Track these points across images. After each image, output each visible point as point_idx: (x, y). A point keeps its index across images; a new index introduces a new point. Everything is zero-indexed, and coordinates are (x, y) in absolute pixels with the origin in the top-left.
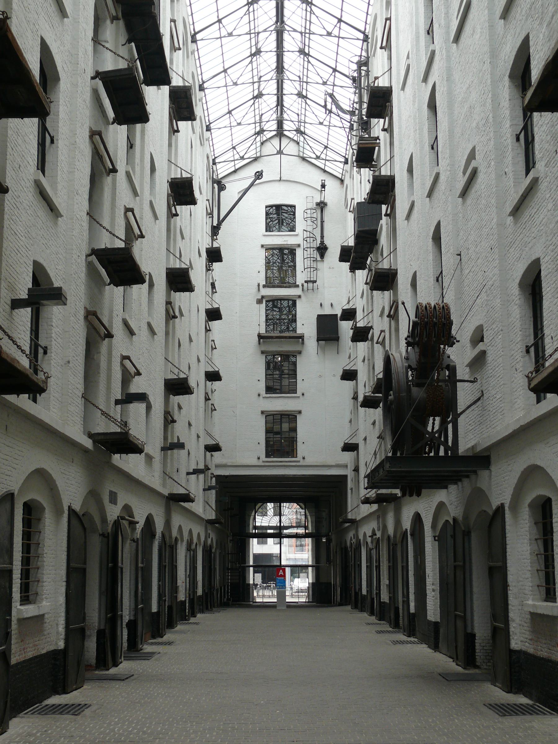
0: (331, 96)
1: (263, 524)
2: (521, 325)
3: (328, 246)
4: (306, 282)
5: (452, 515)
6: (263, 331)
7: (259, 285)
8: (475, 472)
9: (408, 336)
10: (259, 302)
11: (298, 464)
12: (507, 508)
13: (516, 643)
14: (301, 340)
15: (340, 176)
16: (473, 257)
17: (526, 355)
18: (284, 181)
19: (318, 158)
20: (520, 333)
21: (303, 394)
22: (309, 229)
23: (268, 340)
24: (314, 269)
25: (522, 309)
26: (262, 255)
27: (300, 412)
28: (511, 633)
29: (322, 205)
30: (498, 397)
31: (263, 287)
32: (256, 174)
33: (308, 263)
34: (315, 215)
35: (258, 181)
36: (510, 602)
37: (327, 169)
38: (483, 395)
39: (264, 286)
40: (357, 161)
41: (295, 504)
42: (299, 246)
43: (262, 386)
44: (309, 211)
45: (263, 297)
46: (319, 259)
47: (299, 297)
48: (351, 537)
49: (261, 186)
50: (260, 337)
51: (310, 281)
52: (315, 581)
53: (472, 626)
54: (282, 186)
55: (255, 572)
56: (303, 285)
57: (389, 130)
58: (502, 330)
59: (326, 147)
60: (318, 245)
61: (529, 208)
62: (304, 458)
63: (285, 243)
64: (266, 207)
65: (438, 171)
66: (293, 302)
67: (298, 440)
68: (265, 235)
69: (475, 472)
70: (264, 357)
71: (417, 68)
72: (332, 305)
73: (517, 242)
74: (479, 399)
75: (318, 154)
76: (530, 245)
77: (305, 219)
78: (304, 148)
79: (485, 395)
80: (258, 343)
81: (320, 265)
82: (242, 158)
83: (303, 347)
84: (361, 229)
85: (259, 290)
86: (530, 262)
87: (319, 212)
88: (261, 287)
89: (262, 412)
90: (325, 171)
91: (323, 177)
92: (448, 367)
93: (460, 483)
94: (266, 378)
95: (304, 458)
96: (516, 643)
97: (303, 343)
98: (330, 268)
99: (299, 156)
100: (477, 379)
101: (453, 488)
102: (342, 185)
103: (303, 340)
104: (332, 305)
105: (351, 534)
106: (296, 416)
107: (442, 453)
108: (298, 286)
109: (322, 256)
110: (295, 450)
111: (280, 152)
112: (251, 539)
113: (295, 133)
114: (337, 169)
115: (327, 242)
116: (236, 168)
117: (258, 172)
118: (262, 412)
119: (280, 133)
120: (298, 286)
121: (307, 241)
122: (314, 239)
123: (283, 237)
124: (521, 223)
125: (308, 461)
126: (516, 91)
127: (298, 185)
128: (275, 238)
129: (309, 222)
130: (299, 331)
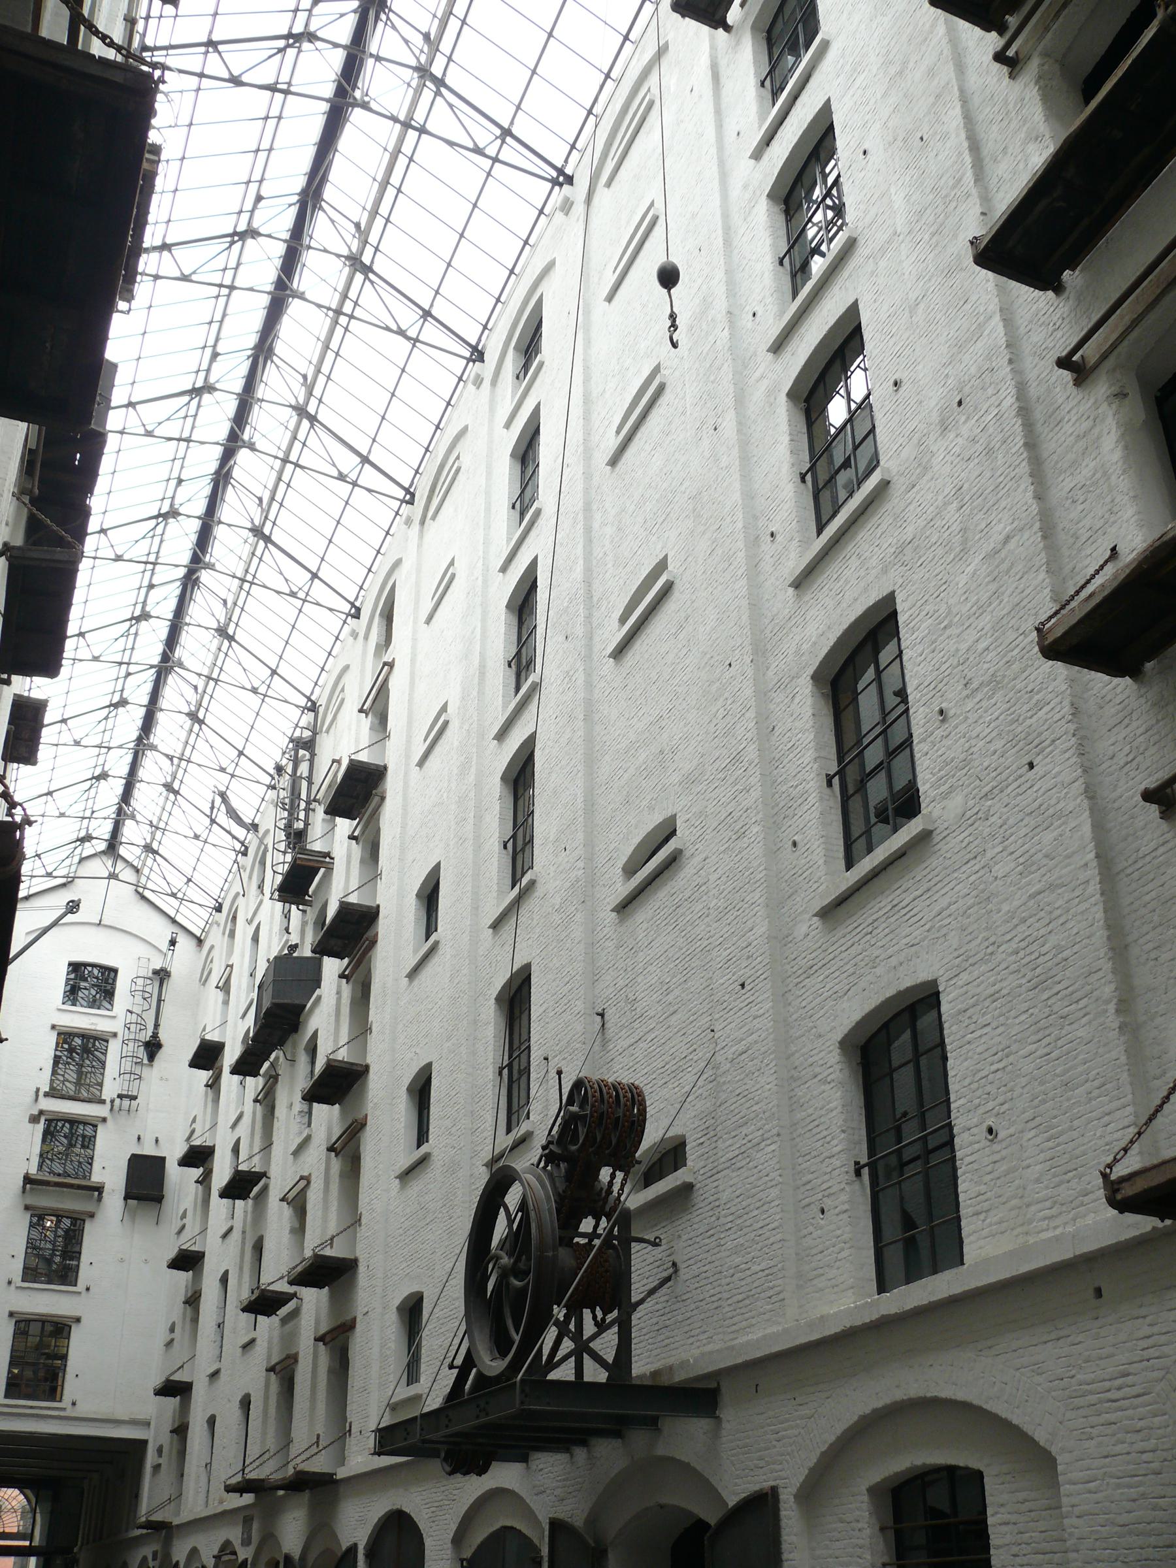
2: (845, 1121)
3: (162, 1042)
4: (120, 1096)
6: (33, 1170)
7: (38, 1090)
10: (34, 1119)
11: (62, 1414)
12: (787, 1499)
14: (96, 1193)
17: (855, 1179)
18: (106, 926)
20: (843, 1135)
21: (88, 1289)
22: (137, 1010)
23: (40, 1187)
24: (137, 1077)
25: (847, 1091)
26: (51, 1040)
27: (78, 1320)
29: (162, 975)
31: (45, 1096)
32: (68, 903)
33: (127, 1065)
34: (149, 989)
35: (70, 918)
37: (179, 918)
38: (676, 1271)
39: (46, 1095)
41: (17, 1492)
42: (115, 1035)
43: (18, 1266)
45: (41, 1112)
46: (146, 1061)
47: (104, 1120)
49: (66, 928)
51: (127, 1096)
54: (102, 933)
56: (112, 1101)
58: (778, 1135)
59: (315, 576)
60: (148, 1039)
61: (887, 892)
62: (74, 1404)
63: (93, 1027)
65: (534, 878)
66: (93, 1124)
67: (68, 1369)
68: (59, 1010)
70: (28, 1215)
71: (478, 720)
72: (157, 1141)
74: (668, 1279)
75: (295, 589)
77: (132, 993)
78: (148, 878)
79: (682, 1272)
80: (21, 1190)
81: (146, 1072)
82: (49, 875)
83: (99, 1205)
84: (276, 1001)
85: (36, 1100)
87: (157, 984)
88: (41, 1094)
90: (174, 921)
91: (175, 929)
93: (580, 1453)
94: (26, 1253)
95: (74, 1404)
98: (161, 1079)
100: (661, 1240)
102: (198, 948)
104: (157, 1141)
106: (70, 1327)
108: (103, 1102)
109: (151, 1057)
110: (59, 1389)
114: (194, 918)
115: (163, 1036)
116: (31, 893)
117: (72, 901)
118: (11, 1314)
120: (103, 1102)
121: (129, 1029)
122: (143, 1027)
123: (91, 1017)
124: (855, 925)
125: (83, 1410)
126: (823, 703)
128: (76, 1016)
129: (138, 999)
130: (96, 1177)
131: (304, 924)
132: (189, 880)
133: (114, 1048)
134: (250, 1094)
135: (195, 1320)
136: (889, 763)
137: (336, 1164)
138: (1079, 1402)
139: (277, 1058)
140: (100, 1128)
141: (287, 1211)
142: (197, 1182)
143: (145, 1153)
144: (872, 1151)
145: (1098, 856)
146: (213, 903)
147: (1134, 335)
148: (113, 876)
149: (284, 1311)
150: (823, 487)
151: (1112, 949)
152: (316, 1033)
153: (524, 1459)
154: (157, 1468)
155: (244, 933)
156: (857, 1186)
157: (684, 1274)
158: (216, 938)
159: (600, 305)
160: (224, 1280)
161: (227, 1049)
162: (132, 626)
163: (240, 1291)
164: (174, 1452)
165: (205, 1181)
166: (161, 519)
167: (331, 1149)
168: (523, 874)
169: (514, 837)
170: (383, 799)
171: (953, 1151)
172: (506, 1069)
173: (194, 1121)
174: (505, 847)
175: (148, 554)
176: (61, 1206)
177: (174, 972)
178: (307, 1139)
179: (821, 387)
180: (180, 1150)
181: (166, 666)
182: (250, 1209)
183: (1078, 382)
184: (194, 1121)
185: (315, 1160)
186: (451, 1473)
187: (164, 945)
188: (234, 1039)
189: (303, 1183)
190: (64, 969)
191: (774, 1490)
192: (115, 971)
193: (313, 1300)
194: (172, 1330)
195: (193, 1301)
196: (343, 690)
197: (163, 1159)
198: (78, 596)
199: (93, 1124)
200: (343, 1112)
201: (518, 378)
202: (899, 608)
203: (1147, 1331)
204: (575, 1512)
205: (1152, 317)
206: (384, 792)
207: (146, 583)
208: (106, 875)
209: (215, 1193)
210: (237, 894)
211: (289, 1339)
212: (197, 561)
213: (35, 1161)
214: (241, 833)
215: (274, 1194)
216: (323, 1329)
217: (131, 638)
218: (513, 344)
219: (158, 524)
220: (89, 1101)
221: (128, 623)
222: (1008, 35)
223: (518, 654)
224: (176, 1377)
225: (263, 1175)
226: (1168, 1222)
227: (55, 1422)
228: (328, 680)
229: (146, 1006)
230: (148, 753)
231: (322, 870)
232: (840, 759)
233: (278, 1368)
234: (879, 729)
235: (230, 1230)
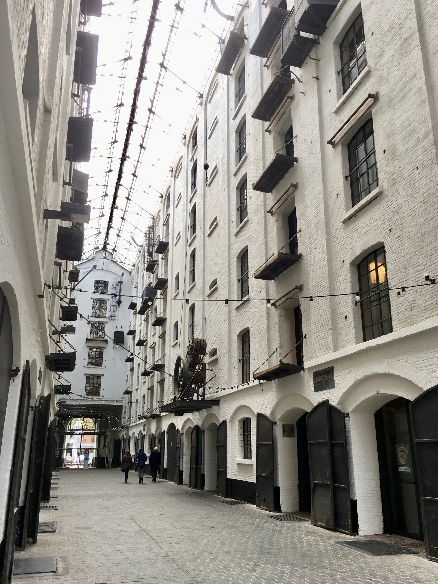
0: (132, 238)
1: (74, 428)
3: (122, 301)
4: (111, 316)
5: (195, 424)
6: (89, 337)
7: (89, 316)
8: (211, 407)
9: (188, 351)
12: (227, 422)
13: (230, 476)
15: (130, 271)
16: (213, 321)
19: (122, 262)
21: (105, 367)
27: (103, 375)
28: (227, 473)
29: (121, 283)
30: (225, 378)
33: (112, 308)
34: (117, 287)
36: (227, 460)
37: (124, 267)
38: (215, 376)
39: (91, 316)
40: (146, 269)
42: (109, 300)
44: (115, 285)
46: (117, 306)
47: (107, 322)
48: (123, 435)
50: (87, 339)
51: (113, 316)
52: (96, 456)
53: (204, 470)
55: (67, 452)
56: (109, 317)
57: (166, 259)
62: (103, 397)
63: (103, 298)
64: (95, 281)
66: (104, 323)
69: (211, 407)
72: (122, 327)
73: (237, 320)
74: (214, 377)
76: (244, 322)
77: (113, 288)
81: (118, 309)
86: (244, 328)
87: (119, 285)
88: (90, 316)
89: (85, 374)
90: (123, 268)
92: (202, 364)
93: (201, 411)
95: (103, 397)
96: (230, 476)
97: (107, 343)
99: (112, 260)
101: (196, 414)
103: (107, 342)
104: (122, 327)
105: (123, 433)
107: (195, 398)
108: (107, 318)
109: (119, 305)
111: (105, 258)
112: (67, 436)
113: (112, 250)
118: (85, 374)
119: (104, 248)
120: (107, 318)
127: (111, 273)
131: (153, 277)
132: (126, 258)
133: (109, 302)
134: (143, 319)
135: (133, 375)
136: (368, 171)
137: (161, 340)
138: (260, 408)
139: (148, 311)
140: (106, 324)
141: (151, 350)
142: (132, 339)
143: (118, 331)
144: (243, 357)
145: (267, 312)
146: (133, 264)
147: (279, 209)
148: (105, 258)
149: (151, 375)
150: (346, 76)
151: (267, 330)
152: (156, 306)
153: (192, 413)
154: (125, 412)
155: (141, 274)
156: (239, 364)
157: (217, 377)
158: (134, 273)
159: (208, 140)
160: (139, 365)
161: (138, 305)
162: (112, 145)
163: (142, 370)
164: (129, 408)
165: (134, 339)
166: (118, 107)
167: (159, 337)
168: (244, 218)
169: (241, 207)
170: (168, 251)
171: (389, 297)
172: (349, 177)
173: (131, 322)
174: (191, 273)
175: (115, 120)
176: (96, 346)
177: (124, 281)
178: (155, 333)
179: (346, 38)
180: (127, 331)
181: (124, 158)
182: (144, 348)
183: (272, 215)
184: (131, 322)
185: (156, 339)
186: (176, 416)
187: (121, 275)
188: (139, 302)
189: (154, 344)
190: (94, 282)
191: (226, 420)
192: (108, 282)
193: (156, 373)
194: (128, 377)
195: (132, 370)
196: (181, 164)
197: (124, 332)
198: (93, 140)
199: (104, 323)
200: (162, 328)
201: (193, 147)
202: (249, 249)
203: (267, 397)
204: (199, 424)
205: (282, 207)
206: (168, 249)
207: (115, 130)
208: (103, 258)
209: (150, 324)
210: (138, 263)
211: (152, 382)
212: (132, 122)
213: (89, 334)
214: (139, 248)
215: (149, 346)
216: (159, 380)
217: (112, 149)
218: (192, 137)
219: (117, 109)
220: (103, 317)
221: (102, 197)
222: (271, 121)
223: (240, 148)
224: (128, 390)
225: (146, 340)
226: (264, 381)
227: (98, 401)
228: (135, 262)
229: (117, 292)
230: (120, 187)
231: (156, 265)
232: (242, 276)
233: (278, 304)
234: (365, 159)
235: (140, 353)
